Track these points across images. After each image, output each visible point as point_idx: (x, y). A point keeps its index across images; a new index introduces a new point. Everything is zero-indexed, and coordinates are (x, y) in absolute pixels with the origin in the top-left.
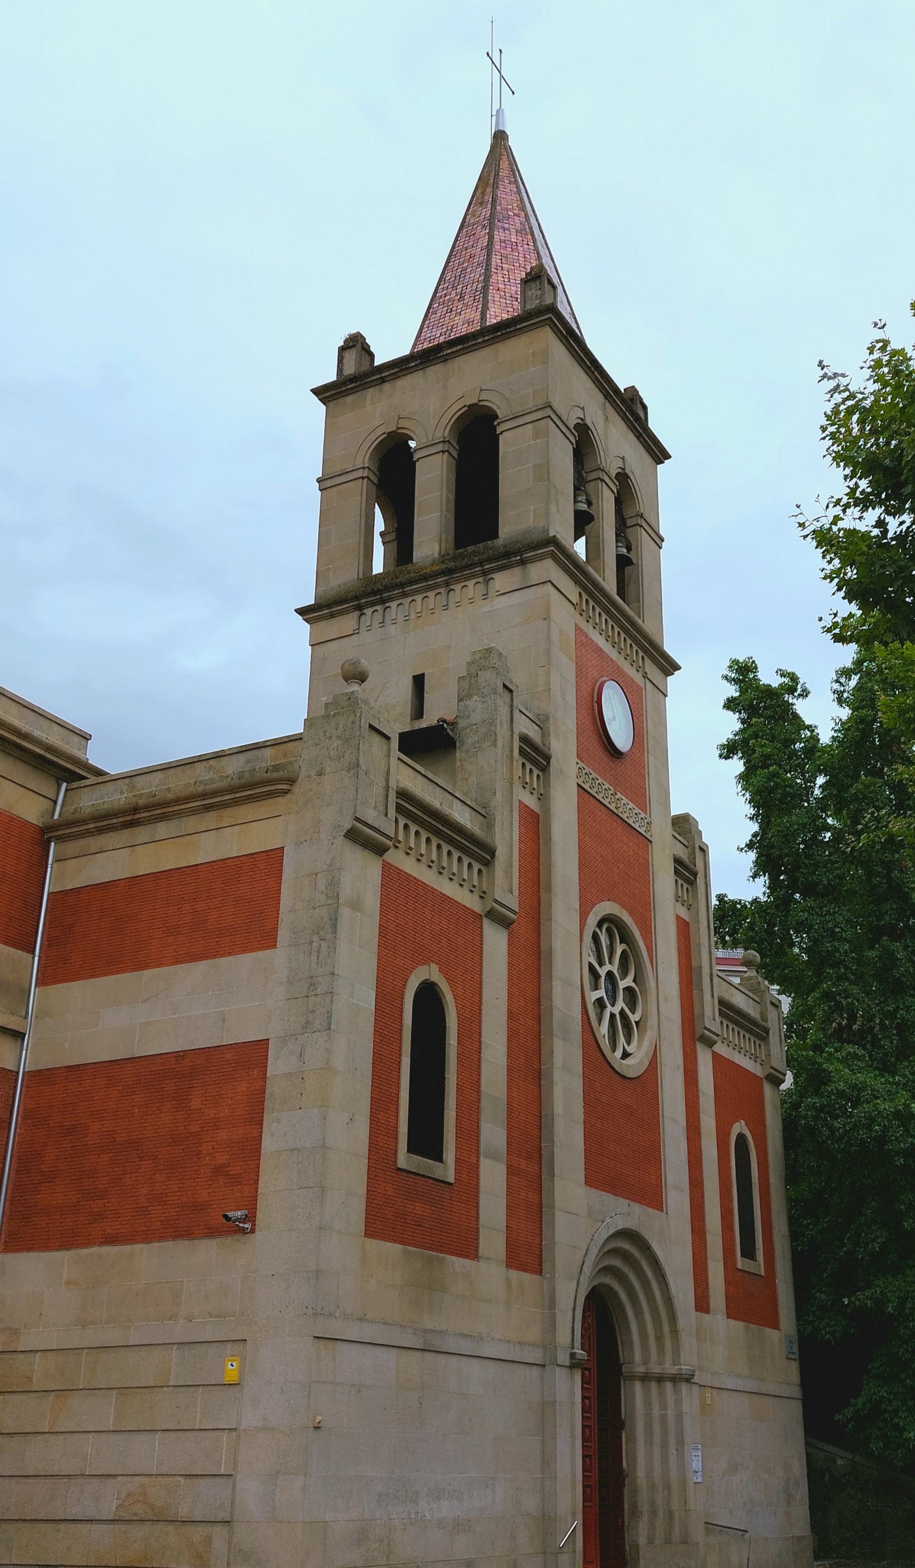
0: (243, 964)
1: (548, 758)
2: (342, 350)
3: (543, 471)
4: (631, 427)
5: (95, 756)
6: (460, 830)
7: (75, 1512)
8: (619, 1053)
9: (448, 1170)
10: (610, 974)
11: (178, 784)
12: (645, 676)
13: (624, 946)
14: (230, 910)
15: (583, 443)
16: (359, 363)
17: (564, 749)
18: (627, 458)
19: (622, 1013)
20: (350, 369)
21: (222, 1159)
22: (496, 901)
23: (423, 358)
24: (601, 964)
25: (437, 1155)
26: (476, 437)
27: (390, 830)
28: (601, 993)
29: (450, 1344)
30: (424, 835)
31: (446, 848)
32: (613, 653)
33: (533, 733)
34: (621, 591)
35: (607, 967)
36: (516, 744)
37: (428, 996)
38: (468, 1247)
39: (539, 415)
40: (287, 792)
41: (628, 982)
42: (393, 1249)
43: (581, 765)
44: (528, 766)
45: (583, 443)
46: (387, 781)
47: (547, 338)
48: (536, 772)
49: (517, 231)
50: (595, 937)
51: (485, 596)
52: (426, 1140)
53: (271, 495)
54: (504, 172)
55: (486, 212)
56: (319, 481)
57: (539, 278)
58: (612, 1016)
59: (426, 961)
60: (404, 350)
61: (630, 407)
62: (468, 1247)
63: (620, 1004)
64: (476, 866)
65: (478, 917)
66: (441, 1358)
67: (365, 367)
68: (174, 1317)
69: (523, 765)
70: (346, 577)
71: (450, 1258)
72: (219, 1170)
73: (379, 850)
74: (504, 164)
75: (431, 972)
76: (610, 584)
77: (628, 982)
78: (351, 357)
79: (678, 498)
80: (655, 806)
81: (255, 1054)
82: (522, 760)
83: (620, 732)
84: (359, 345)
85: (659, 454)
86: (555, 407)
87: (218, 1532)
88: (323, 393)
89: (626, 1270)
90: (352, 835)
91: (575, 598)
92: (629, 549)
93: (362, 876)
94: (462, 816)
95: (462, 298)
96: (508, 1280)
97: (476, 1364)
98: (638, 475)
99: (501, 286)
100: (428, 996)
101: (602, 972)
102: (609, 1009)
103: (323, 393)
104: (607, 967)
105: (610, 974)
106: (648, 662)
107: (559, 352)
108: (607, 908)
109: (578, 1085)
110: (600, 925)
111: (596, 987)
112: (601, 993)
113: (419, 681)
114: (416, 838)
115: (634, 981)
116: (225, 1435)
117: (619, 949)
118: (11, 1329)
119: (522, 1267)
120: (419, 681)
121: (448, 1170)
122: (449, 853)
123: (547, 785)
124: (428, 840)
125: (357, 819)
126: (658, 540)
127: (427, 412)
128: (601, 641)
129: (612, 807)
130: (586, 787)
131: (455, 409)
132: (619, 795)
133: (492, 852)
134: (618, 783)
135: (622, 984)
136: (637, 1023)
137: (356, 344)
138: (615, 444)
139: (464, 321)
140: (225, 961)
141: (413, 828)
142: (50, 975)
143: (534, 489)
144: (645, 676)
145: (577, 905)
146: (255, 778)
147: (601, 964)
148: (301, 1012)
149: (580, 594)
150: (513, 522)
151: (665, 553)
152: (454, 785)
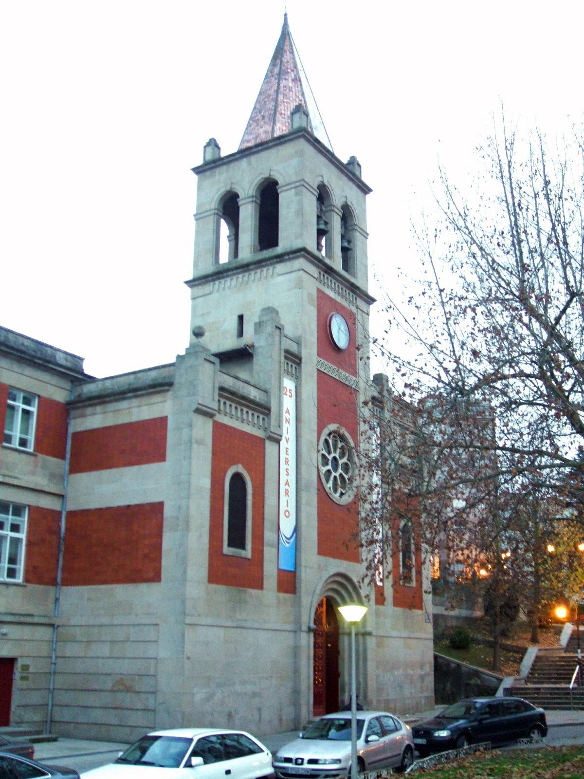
0: (154, 467)
1: (300, 360)
2: (205, 147)
3: (300, 212)
4: (350, 179)
5: (88, 370)
6: (253, 402)
7: (96, 687)
8: (338, 494)
9: (248, 553)
10: (335, 458)
11: (124, 383)
12: (357, 307)
13: (343, 444)
14: (146, 444)
15: (323, 195)
16: (214, 153)
17: (310, 353)
18: (348, 197)
19: (341, 475)
20: (209, 157)
21: (146, 551)
22: (271, 432)
23: (244, 153)
24: (329, 453)
25: (243, 546)
26: (269, 193)
27: (216, 406)
28: (329, 467)
29: (249, 624)
30: (234, 406)
31: (245, 410)
32: (339, 299)
33: (294, 348)
34: (346, 267)
35: (333, 455)
36: (283, 353)
37: (237, 478)
38: (258, 584)
39: (298, 184)
40: (168, 390)
41: (345, 460)
42: (222, 588)
43: (319, 359)
44: (290, 363)
45: (323, 195)
46: (214, 384)
47: (302, 144)
48: (294, 366)
49: (293, 80)
50: (326, 441)
51: (272, 276)
52: (237, 540)
53: (173, 228)
54: (287, 48)
55: (276, 70)
56: (195, 215)
57: (300, 110)
58: (335, 477)
59: (235, 463)
60: (235, 150)
61: (350, 171)
62: (258, 584)
63: (340, 471)
64: (261, 416)
65: (262, 441)
66: (244, 631)
67: (217, 156)
68: (130, 614)
69: (287, 363)
70: (208, 268)
71: (248, 589)
72: (146, 556)
73: (211, 416)
74: (287, 43)
75: (239, 468)
76: (337, 264)
77: (345, 460)
78: (209, 150)
79: (375, 214)
80: (361, 373)
81: (157, 508)
82: (286, 361)
83: (341, 338)
84: (213, 144)
85: (365, 189)
86: (307, 180)
87: (151, 697)
88: (198, 170)
89: (343, 592)
90: (198, 411)
91: (316, 275)
92: (349, 242)
93: (204, 429)
94: (254, 394)
95: (263, 117)
96: (278, 598)
97: (263, 633)
98: (354, 202)
99: (283, 112)
100: (237, 478)
101: (330, 457)
102: (334, 474)
103: (198, 170)
104: (333, 455)
105: (335, 458)
106: (358, 299)
107: (310, 150)
108: (333, 427)
109: (314, 511)
110: (329, 435)
111: (327, 464)
112: (329, 467)
113: (241, 318)
114: (229, 407)
115: (348, 460)
116: (152, 661)
117: (340, 445)
118: (53, 625)
119: (286, 592)
120: (241, 318)
121: (248, 553)
122: (247, 412)
123: (300, 371)
124: (236, 408)
125: (199, 404)
126: (365, 235)
127: (245, 181)
128: (332, 294)
129: (337, 378)
130: (322, 370)
131: (258, 179)
132: (341, 370)
133: (269, 410)
134: (340, 365)
135: (341, 462)
136: (349, 479)
137: (213, 144)
138: (341, 191)
139: (263, 133)
140: (145, 467)
141: (228, 403)
142: (75, 469)
143: (296, 223)
144: (357, 307)
145: (315, 428)
146: (157, 383)
147: (329, 453)
148: (179, 485)
149: (320, 273)
150: (287, 239)
151: (369, 241)
152: (252, 377)
